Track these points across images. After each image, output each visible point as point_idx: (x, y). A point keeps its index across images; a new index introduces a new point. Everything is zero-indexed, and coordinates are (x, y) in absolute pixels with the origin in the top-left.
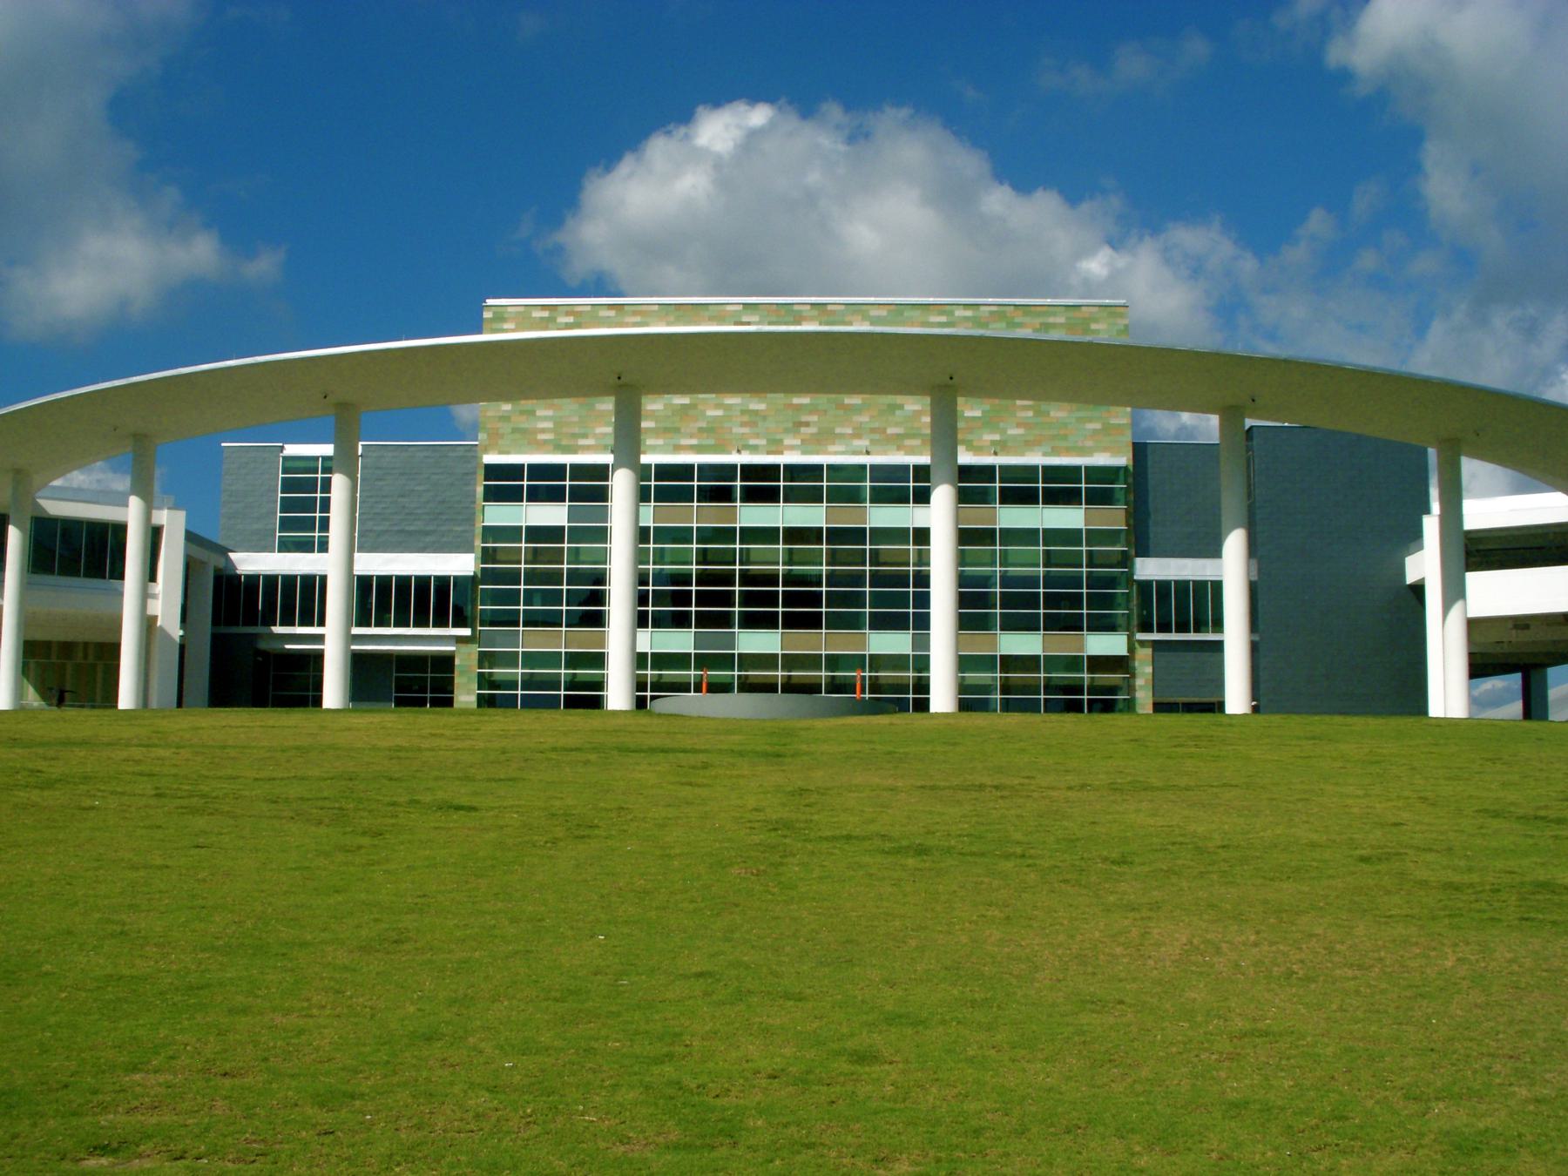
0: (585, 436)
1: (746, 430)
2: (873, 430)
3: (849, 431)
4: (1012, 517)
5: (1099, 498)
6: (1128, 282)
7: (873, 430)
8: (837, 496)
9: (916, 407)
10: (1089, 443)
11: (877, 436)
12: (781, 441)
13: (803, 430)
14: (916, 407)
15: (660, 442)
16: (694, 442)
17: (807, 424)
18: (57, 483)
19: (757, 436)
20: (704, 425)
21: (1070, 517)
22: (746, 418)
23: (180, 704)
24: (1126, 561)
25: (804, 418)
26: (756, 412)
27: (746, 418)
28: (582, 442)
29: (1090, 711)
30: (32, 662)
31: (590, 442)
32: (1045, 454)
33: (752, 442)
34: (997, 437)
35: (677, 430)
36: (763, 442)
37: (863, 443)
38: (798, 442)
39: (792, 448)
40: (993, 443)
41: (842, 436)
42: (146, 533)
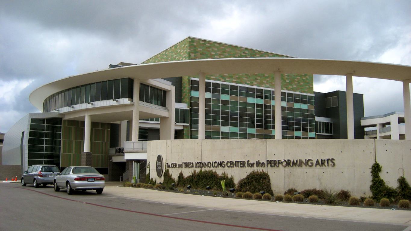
0: (213, 76)
1: (246, 79)
2: (270, 83)
3: (266, 82)
4: (297, 105)
5: (310, 103)
6: (25, 85)
7: (270, 83)
8: (232, 93)
9: (343, 78)
10: (307, 91)
11: (271, 84)
12: (253, 83)
13: (257, 81)
14: (343, 78)
15: (229, 80)
16: (236, 80)
17: (258, 79)
18: (216, 75)
19: (248, 81)
20: (237, 76)
21: (305, 106)
22: (246, 76)
23: (146, 152)
24: (313, 117)
25: (257, 78)
26: (248, 75)
27: (246, 76)
28: (212, 77)
29: (131, 81)
30: (94, 129)
31: (214, 77)
32: (300, 92)
33: (247, 82)
34: (291, 87)
35: (232, 77)
36: (249, 82)
37: (268, 85)
38: (256, 83)
39: (255, 85)
40: (291, 88)
41: (264, 83)
42: (90, 123)
